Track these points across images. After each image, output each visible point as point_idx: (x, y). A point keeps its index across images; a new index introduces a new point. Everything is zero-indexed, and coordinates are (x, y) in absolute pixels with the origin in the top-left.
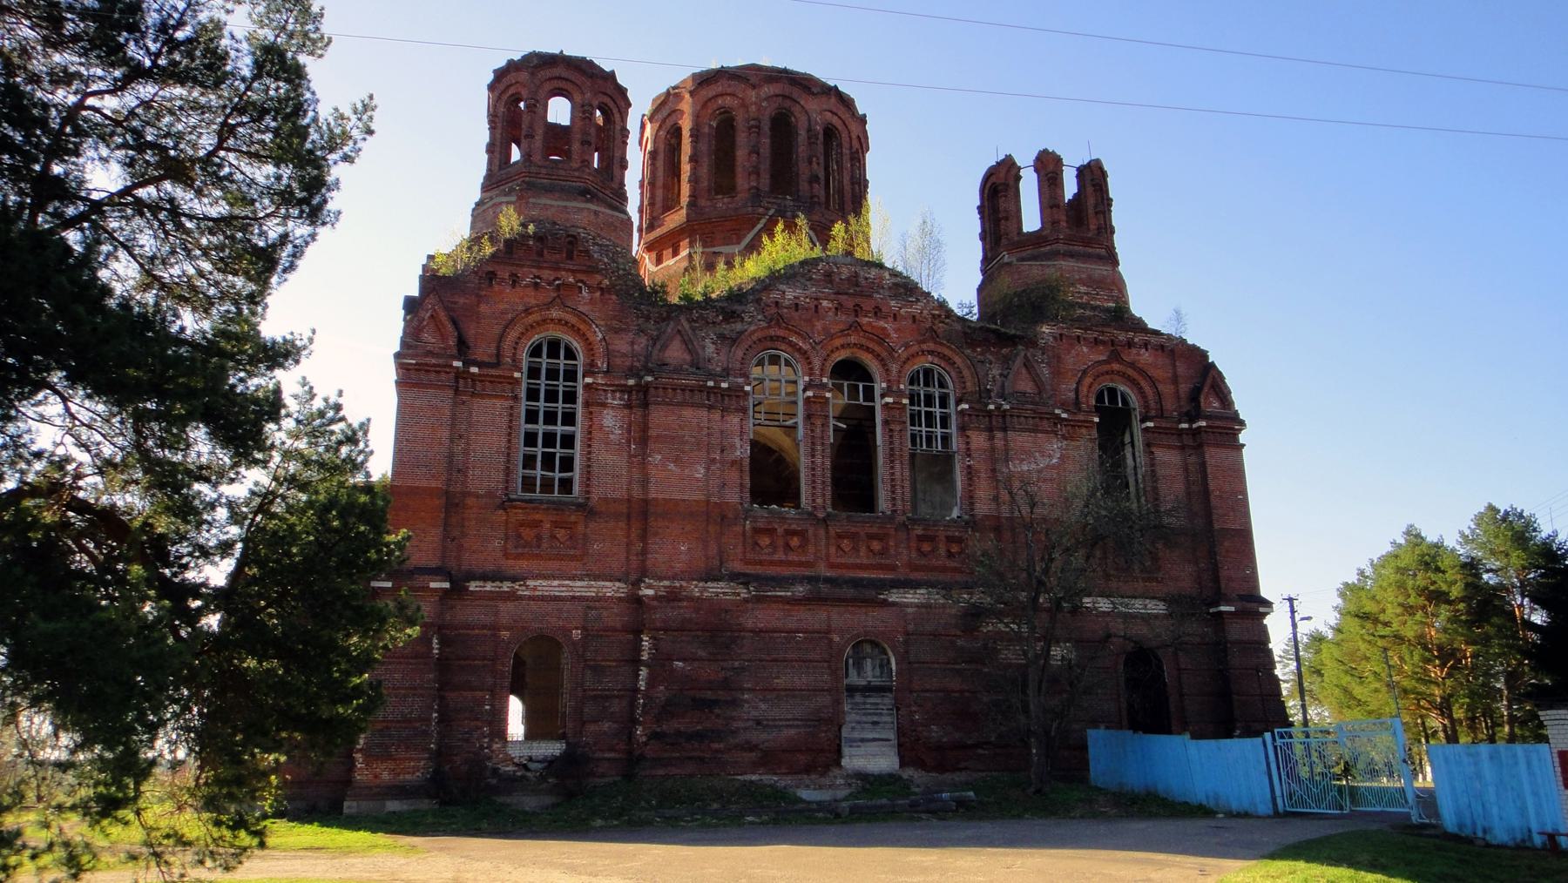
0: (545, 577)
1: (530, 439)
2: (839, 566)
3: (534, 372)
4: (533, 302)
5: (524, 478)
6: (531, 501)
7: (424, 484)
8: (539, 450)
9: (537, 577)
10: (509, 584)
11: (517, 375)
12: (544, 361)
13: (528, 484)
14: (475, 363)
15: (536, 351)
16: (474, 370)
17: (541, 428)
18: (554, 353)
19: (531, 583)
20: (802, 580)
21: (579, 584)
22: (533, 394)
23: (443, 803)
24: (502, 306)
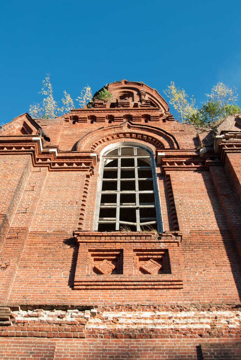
0: (130, 308)
19: (111, 315)
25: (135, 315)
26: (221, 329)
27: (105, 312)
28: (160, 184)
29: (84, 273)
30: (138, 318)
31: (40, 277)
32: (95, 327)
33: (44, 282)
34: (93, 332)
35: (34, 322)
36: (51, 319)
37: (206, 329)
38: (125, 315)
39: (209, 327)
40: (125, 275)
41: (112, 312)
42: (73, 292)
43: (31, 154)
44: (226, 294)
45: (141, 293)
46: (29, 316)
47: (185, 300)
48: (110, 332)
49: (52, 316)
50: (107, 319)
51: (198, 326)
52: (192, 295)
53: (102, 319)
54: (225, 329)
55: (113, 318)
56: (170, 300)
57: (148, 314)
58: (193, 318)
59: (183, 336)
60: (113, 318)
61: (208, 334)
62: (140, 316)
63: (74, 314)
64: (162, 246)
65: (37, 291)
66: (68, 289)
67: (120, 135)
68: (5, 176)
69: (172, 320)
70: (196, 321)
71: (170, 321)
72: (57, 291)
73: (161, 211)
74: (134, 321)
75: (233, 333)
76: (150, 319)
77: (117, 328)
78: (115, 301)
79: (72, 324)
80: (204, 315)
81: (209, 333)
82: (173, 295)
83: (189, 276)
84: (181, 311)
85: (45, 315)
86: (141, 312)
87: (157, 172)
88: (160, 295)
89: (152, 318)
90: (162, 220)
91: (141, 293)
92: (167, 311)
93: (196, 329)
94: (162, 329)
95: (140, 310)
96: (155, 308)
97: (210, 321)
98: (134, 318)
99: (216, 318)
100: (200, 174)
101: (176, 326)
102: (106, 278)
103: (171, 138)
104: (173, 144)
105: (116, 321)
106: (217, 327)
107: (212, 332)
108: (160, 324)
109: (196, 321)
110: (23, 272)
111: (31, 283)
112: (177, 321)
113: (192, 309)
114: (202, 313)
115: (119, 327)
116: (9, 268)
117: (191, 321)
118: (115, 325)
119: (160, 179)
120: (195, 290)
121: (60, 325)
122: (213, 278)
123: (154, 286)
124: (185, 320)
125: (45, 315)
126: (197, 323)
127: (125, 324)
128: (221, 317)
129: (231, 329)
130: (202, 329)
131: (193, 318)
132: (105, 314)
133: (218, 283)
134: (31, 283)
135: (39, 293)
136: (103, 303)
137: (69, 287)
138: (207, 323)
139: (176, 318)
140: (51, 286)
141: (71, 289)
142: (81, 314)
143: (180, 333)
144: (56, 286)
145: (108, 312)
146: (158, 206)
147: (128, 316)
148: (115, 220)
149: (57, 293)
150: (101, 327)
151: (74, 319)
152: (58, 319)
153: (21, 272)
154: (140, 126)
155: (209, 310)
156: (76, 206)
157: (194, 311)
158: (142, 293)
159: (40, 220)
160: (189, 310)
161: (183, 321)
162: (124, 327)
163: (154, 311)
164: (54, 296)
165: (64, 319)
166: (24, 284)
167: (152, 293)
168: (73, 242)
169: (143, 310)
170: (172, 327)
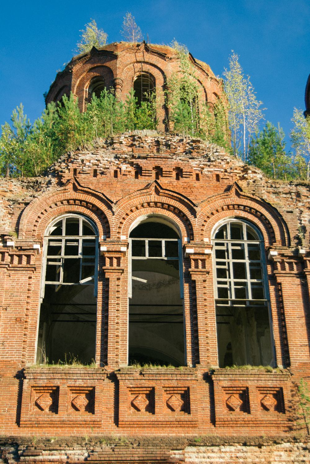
2: (132, 425)
12: (229, 244)
18: (236, 232)
20: (79, 441)
29: (221, 411)
68: (102, 173)
104: (284, 234)
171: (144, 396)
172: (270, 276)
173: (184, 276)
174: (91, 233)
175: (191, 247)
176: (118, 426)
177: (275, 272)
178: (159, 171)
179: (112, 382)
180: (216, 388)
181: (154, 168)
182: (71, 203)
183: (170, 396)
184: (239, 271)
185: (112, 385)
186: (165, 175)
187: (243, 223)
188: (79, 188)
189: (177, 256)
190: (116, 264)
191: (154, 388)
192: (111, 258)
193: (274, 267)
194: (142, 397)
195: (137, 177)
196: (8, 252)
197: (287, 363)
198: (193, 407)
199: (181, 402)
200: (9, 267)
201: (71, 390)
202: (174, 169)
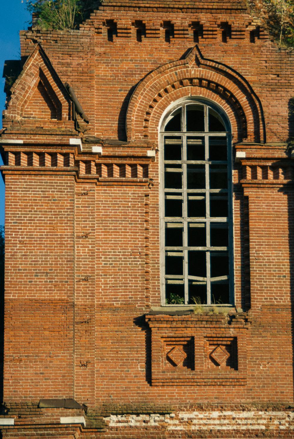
0: (201, 408)
1: (173, 237)
3: (172, 152)
4: (166, 57)
5: (168, 258)
6: (178, 313)
7: (45, 295)
8: (184, 251)
9: (192, 408)
10: (157, 417)
11: (150, 153)
12: (184, 139)
13: (174, 292)
14: (97, 142)
15: (174, 125)
16: (97, 149)
17: (185, 221)
18: (195, 124)
19: (185, 415)
21: (245, 414)
22: (172, 180)
23: (199, 22)
24: (125, 66)
25: (206, 415)
26: (273, 430)
27: (181, 412)
28: (235, 205)
29: (160, 367)
30: (208, 419)
31: (119, 371)
32: (173, 428)
33: (123, 376)
34: (173, 433)
35: (125, 427)
36: (138, 424)
37: (261, 430)
38: (198, 416)
39: (264, 428)
40: (197, 372)
41: (187, 412)
42: (151, 388)
43: (74, 176)
44: (283, 393)
45: (210, 390)
46: (119, 422)
47: (248, 398)
48: (186, 433)
49: (139, 421)
50: (183, 419)
51: (256, 427)
52: (254, 392)
53: (179, 420)
54: (277, 430)
55: (188, 419)
56: (235, 398)
57: (216, 414)
58: (253, 419)
59: (242, 435)
60: (188, 419)
61: (262, 435)
62: (209, 416)
63: (157, 418)
64: (232, 332)
65: (119, 388)
66: (146, 385)
67: (185, 81)
69: (235, 420)
70: (254, 422)
71: (234, 422)
72: (137, 387)
73: (235, 263)
74: (205, 421)
75: (282, 433)
76: (218, 419)
77: (191, 429)
78: (189, 399)
79: (155, 428)
80: (261, 415)
81: (264, 434)
82: (238, 392)
83: (254, 370)
84: (243, 410)
85: (133, 421)
86: (211, 412)
87: (233, 182)
88: (227, 393)
89: (220, 418)
90: (235, 279)
91: (210, 390)
92: (232, 410)
93: (253, 430)
94: (227, 430)
95: (209, 410)
96: (222, 407)
97: (265, 422)
98: (205, 419)
99: (271, 419)
100: (286, 197)
101: (238, 426)
102: (180, 375)
103: (257, 103)
104: (259, 122)
105: (190, 422)
106: (270, 428)
107: (266, 433)
108: (225, 425)
109: (255, 422)
110: (101, 365)
111: (113, 379)
112: (239, 422)
113: (252, 409)
114: (260, 413)
115: (193, 428)
116: (89, 365)
117: (250, 422)
118: (189, 426)
119: (236, 199)
120: (257, 387)
121: (146, 429)
122: (275, 373)
123: (222, 383)
124: (246, 421)
125: (133, 421)
126: (255, 424)
127: (198, 425)
128: (275, 419)
129: (281, 430)
130: (258, 430)
131: (253, 419)
132: (182, 415)
133: (279, 378)
134: (113, 379)
135: (121, 391)
136: (178, 401)
137: (146, 383)
138: (263, 424)
139: (238, 419)
140: (131, 382)
141: (148, 385)
142: (162, 418)
143: (241, 433)
144: (135, 382)
145: (184, 412)
146: (231, 249)
147: (201, 416)
148: (182, 280)
149: (137, 390)
150: (179, 428)
151: (157, 424)
152: (144, 424)
153: (100, 364)
154: (214, 64)
155: (266, 410)
156: (140, 260)
157: (254, 410)
158: (212, 390)
159: (103, 286)
160: (249, 410)
161: (244, 422)
162: (197, 428)
163: (221, 411)
164: (134, 393)
165: (149, 424)
166: (106, 379)
167: (220, 390)
168: (142, 322)
169: (212, 410)
170: (235, 427)
171: (182, 347)
172: (236, 185)
173: (234, 189)
174: (222, 130)
175: (242, 149)
176: (151, 385)
177: (243, 181)
178: (198, 30)
179: (142, 330)
180: (154, 337)
181: (133, 24)
182: (212, 87)
183: (171, 347)
184: (196, 180)
185: (142, 335)
186: (150, 35)
187: (204, 105)
188: (202, 61)
189: (226, 160)
190: (142, 174)
191: (193, 338)
192: (254, 168)
193: (242, 175)
194: (179, 350)
195: (139, 40)
196: (94, 161)
197: (247, 304)
198: (241, 361)
199: (227, 356)
200: (99, 181)
201: (164, 341)
202: (190, 26)
